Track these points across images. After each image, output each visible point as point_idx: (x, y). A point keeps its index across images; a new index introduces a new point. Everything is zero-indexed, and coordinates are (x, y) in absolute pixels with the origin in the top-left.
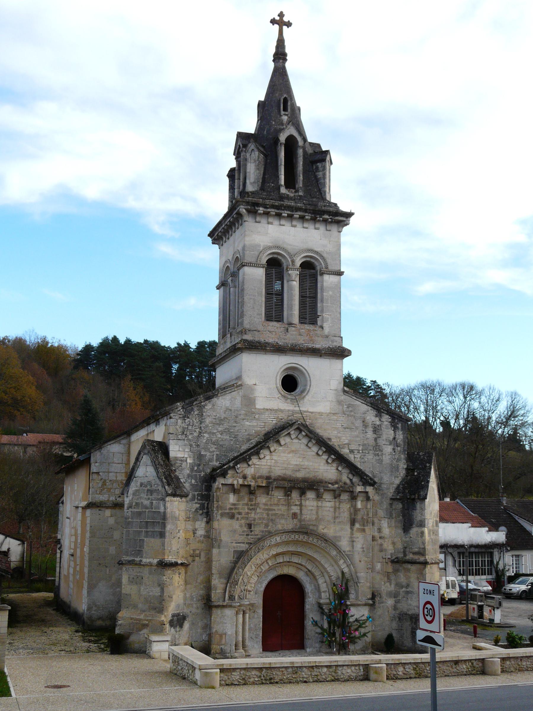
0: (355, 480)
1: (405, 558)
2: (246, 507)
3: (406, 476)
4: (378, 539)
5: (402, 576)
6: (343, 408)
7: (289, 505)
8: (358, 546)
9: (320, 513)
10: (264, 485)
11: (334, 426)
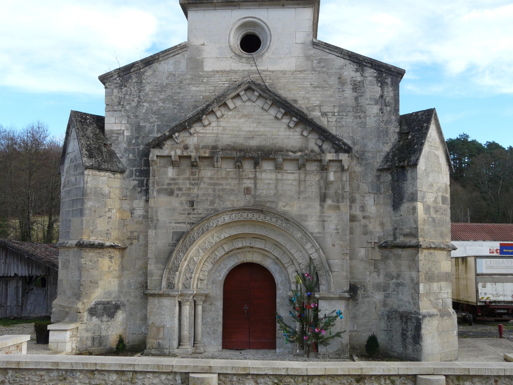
0: (326, 146)
1: (395, 241)
2: (188, 182)
3: (399, 141)
4: (361, 219)
5: (392, 264)
6: (312, 64)
7: (240, 178)
8: (331, 227)
9: (279, 187)
10: (207, 155)
11: (300, 86)
